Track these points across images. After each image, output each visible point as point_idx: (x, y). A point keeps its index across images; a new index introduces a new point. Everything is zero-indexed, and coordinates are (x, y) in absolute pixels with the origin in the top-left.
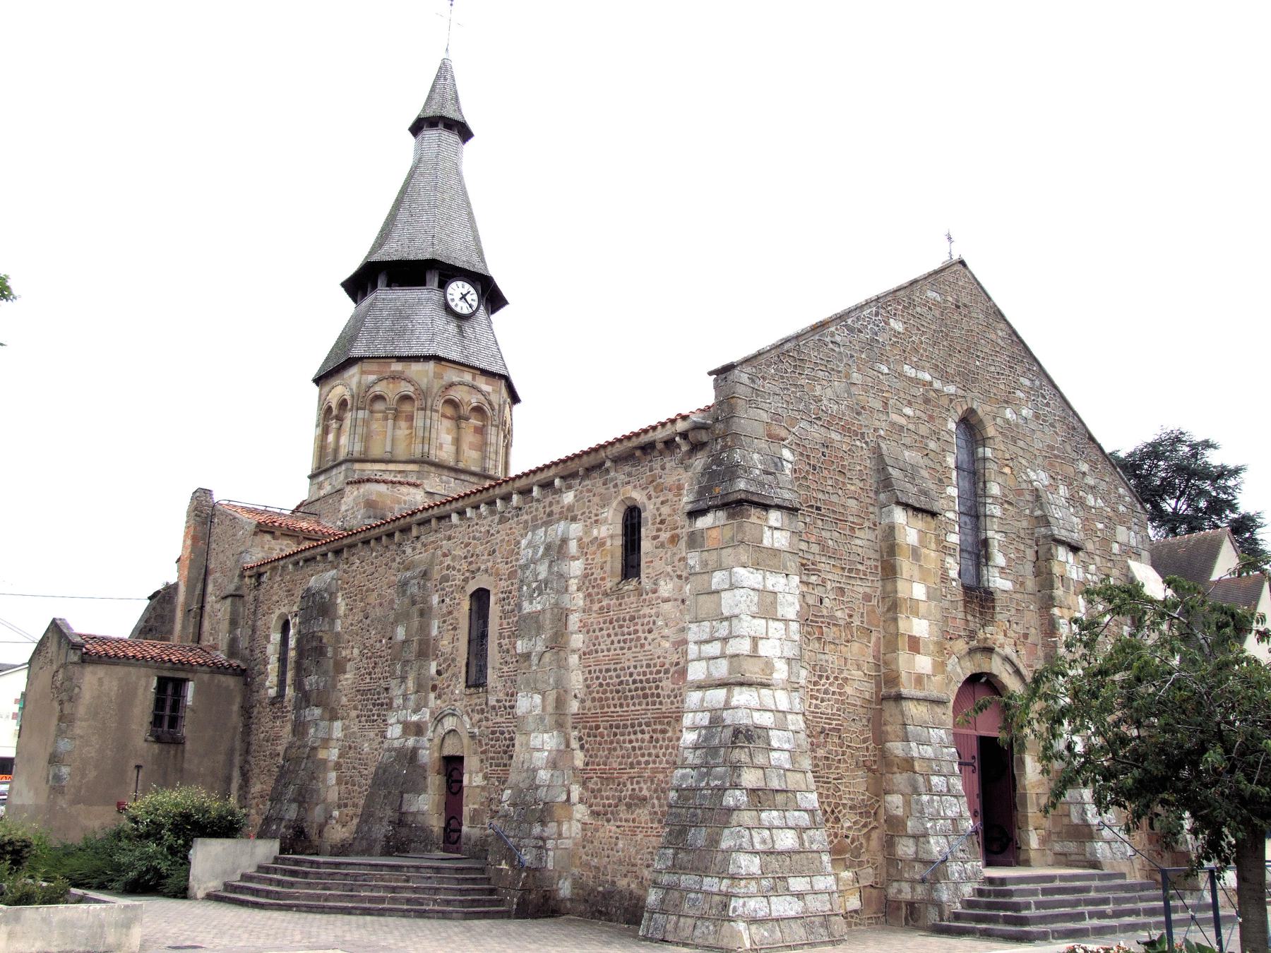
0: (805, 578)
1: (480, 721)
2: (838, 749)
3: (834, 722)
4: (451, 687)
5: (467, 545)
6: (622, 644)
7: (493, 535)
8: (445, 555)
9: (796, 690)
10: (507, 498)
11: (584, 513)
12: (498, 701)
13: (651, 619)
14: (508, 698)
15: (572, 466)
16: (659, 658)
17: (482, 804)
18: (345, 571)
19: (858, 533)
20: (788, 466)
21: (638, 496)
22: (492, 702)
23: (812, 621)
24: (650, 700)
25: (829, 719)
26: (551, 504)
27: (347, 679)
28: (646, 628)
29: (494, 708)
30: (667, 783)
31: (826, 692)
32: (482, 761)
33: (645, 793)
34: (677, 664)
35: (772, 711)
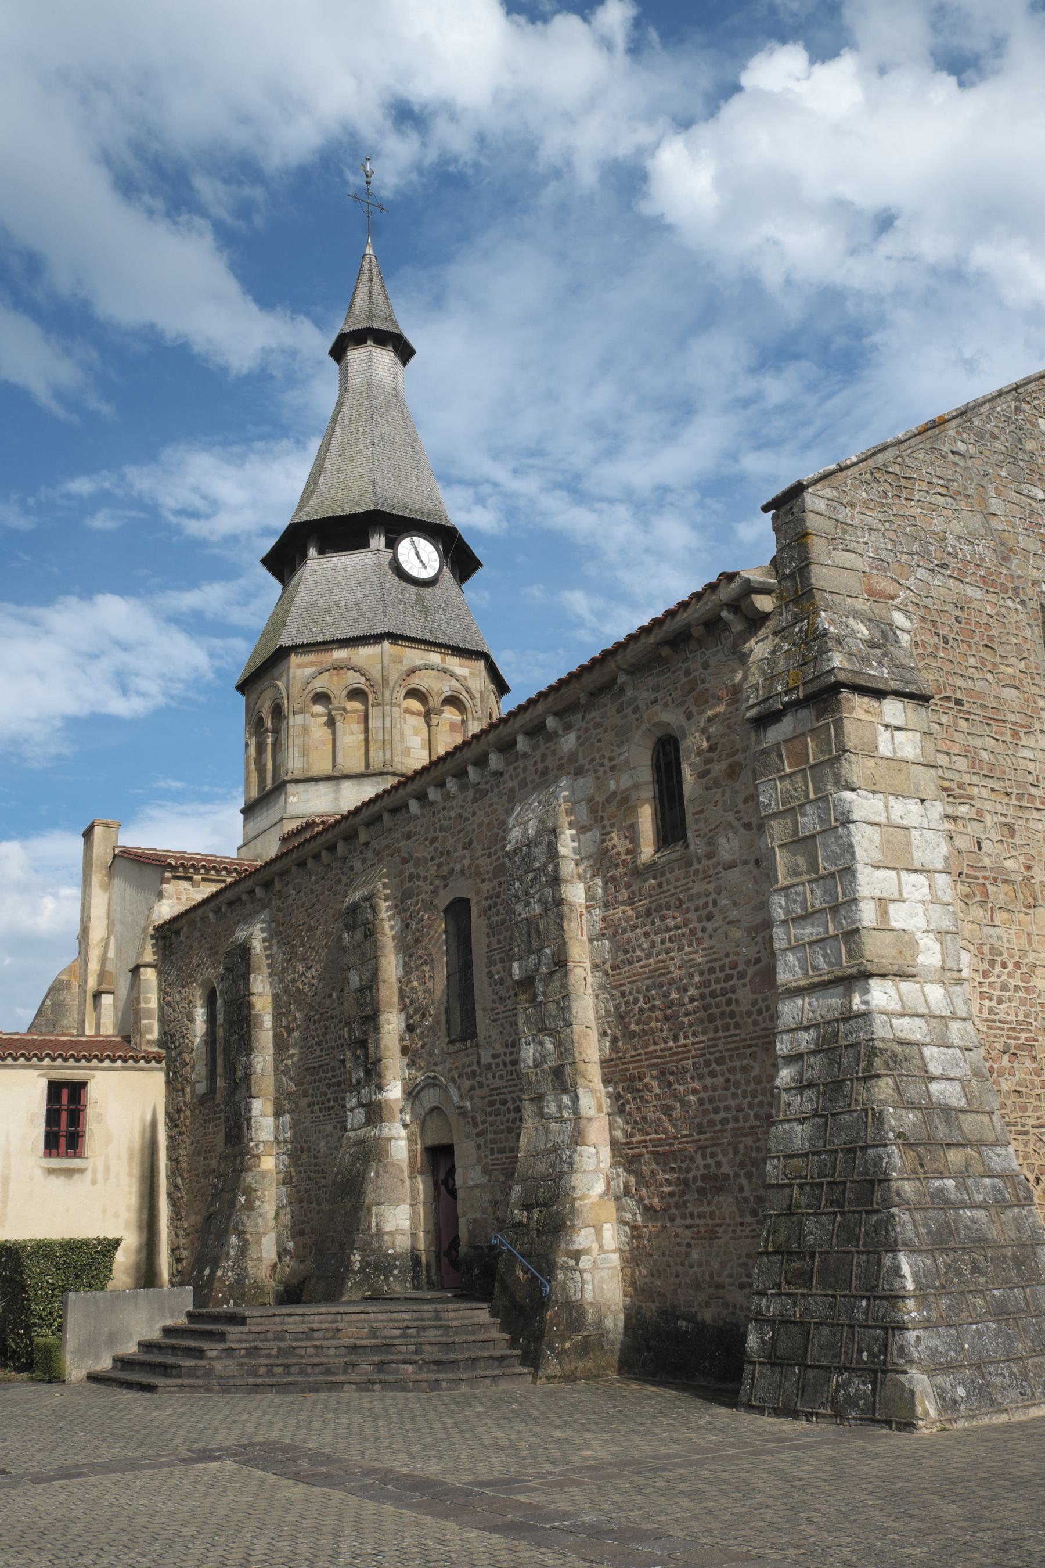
0: (950, 810)
1: (472, 1088)
2: (1034, 1077)
3: (1023, 1035)
4: (428, 1047)
5: (434, 840)
6: (668, 944)
7: (467, 819)
8: (404, 861)
9: (959, 981)
10: (481, 762)
11: (592, 760)
12: (494, 1056)
13: (710, 899)
14: (508, 1051)
15: (569, 693)
16: (727, 955)
17: (484, 1212)
18: (279, 909)
19: (1024, 741)
20: (905, 638)
21: (671, 717)
22: (486, 1057)
23: (968, 876)
24: (719, 1023)
25: (1014, 1029)
26: (544, 757)
27: (292, 1056)
28: (704, 913)
29: (489, 1067)
30: (759, 1150)
31: (1004, 988)
32: (479, 1147)
33: (726, 1169)
34: (758, 961)
35: (922, 1016)
